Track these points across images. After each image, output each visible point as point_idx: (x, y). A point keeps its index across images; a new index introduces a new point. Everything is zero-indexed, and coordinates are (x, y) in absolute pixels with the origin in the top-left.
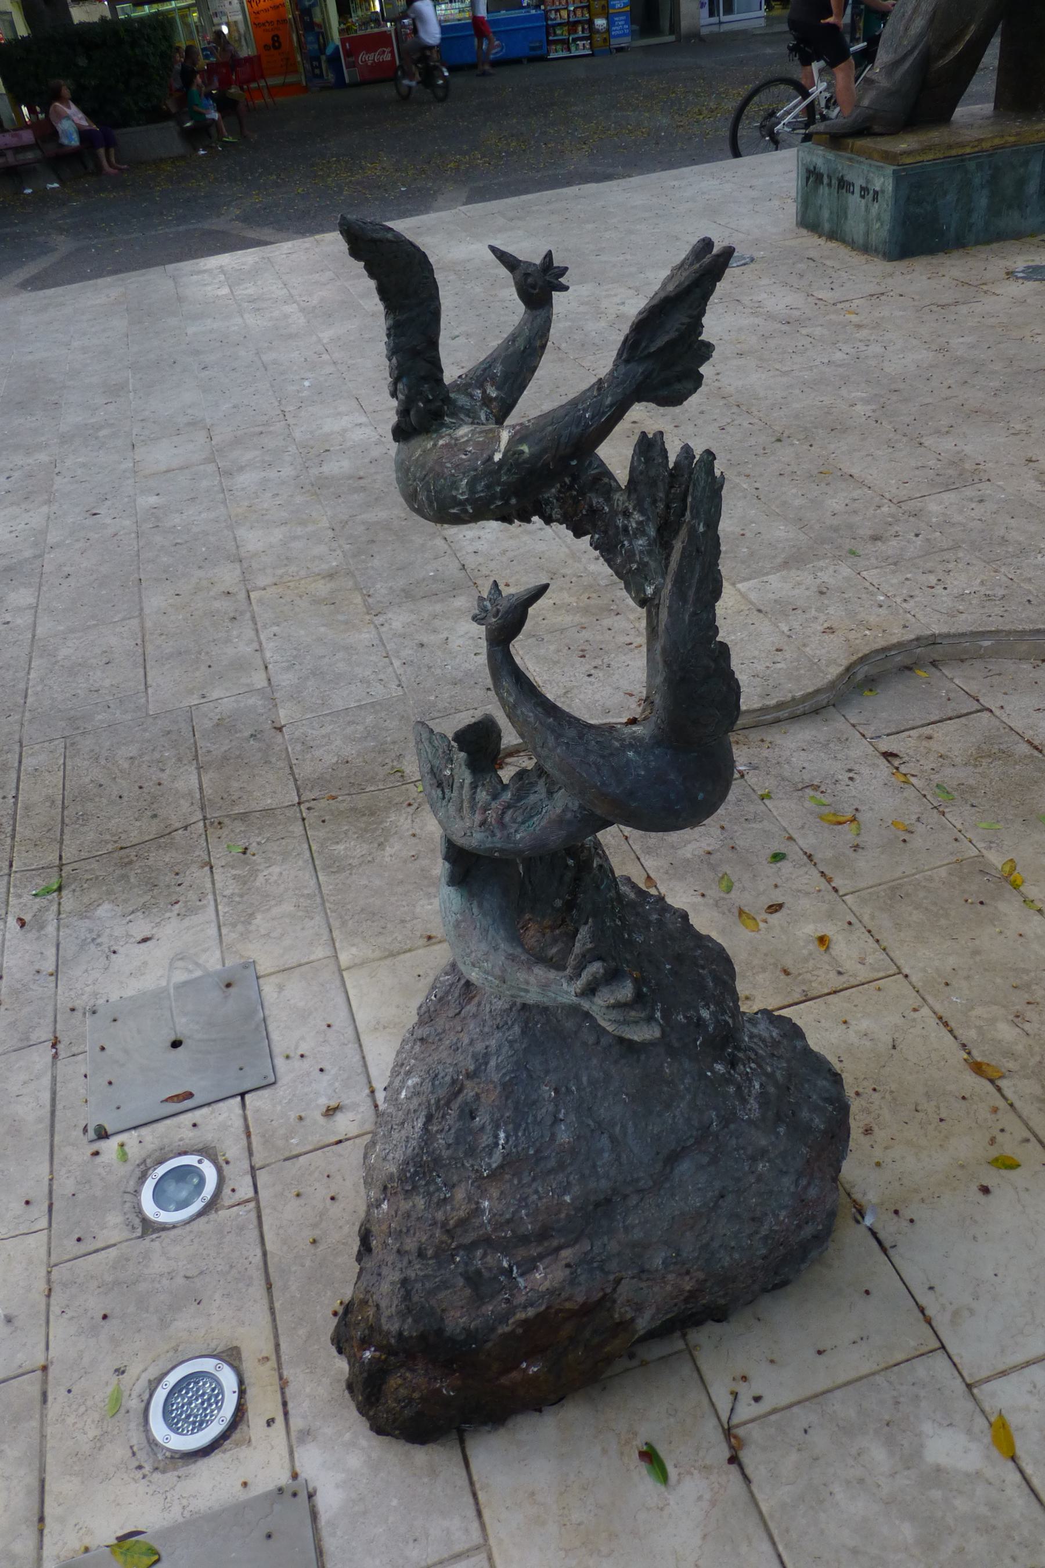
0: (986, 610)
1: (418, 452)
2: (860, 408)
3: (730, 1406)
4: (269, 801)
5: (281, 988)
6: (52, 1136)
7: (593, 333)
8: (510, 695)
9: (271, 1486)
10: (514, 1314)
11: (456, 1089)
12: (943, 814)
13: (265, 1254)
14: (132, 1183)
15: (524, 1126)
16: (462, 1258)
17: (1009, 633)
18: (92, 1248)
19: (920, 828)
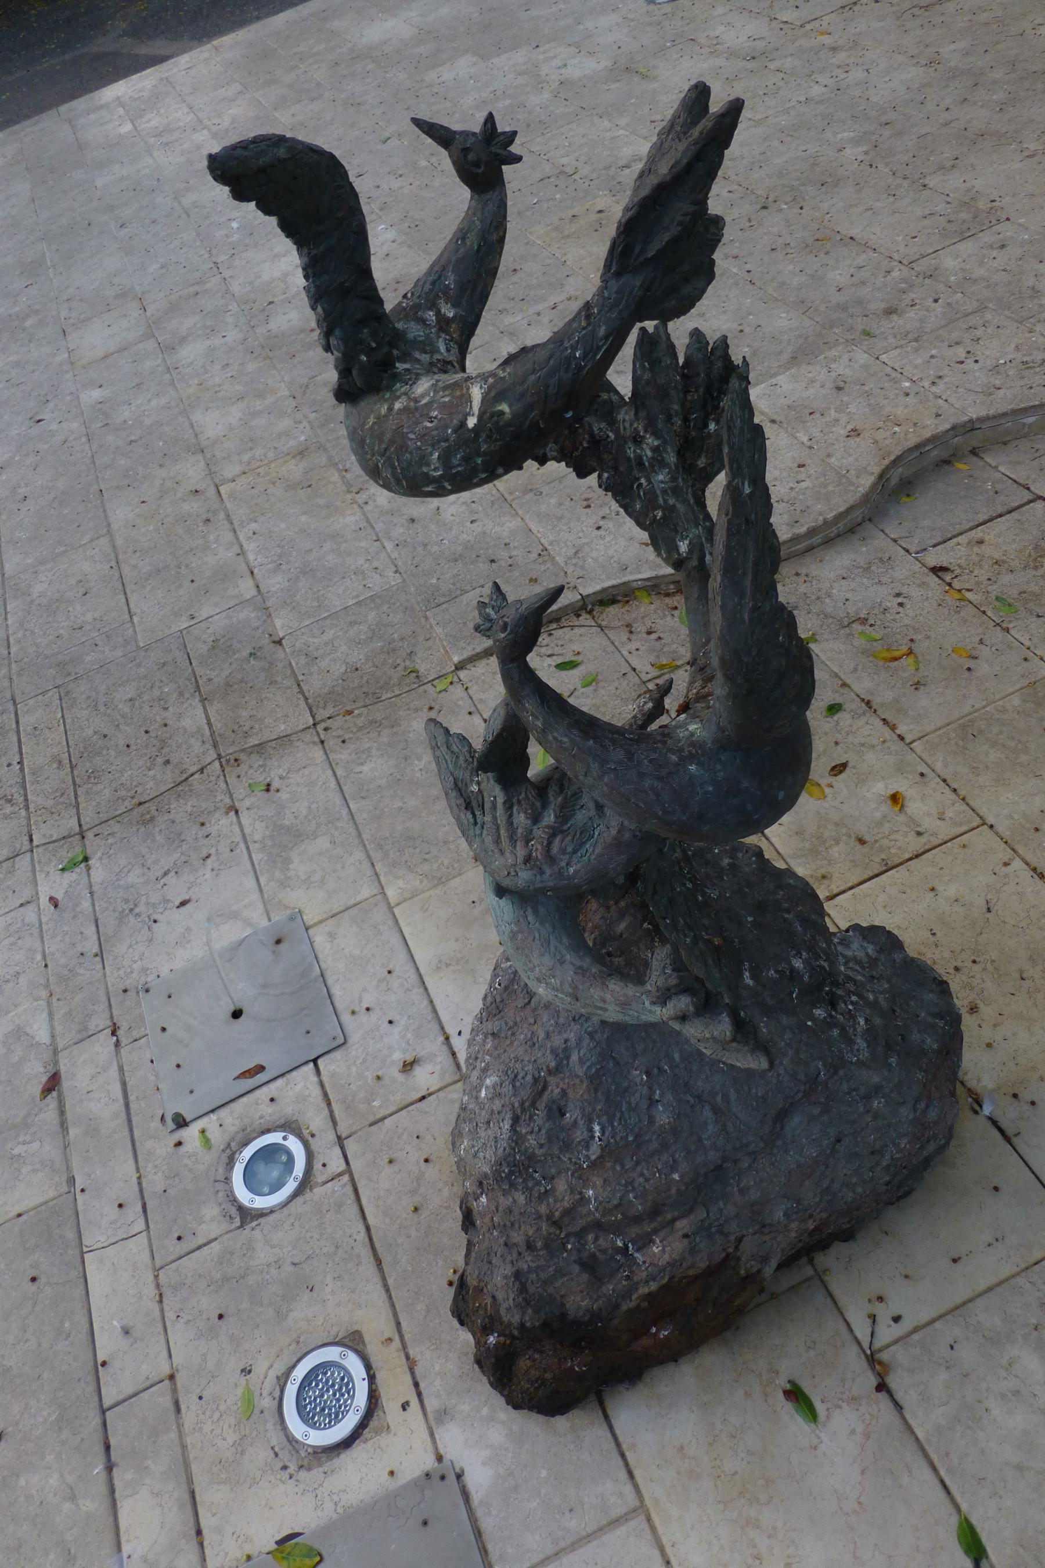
1: (371, 420)
2: (849, 152)
4: (283, 728)
5: (332, 936)
6: (131, 1130)
7: (538, 108)
8: (536, 718)
9: (418, 1472)
10: (637, 1289)
11: (540, 1086)
12: (1007, 630)
13: (368, 1229)
14: (221, 1170)
15: (618, 1115)
18: (194, 1246)
19: (985, 652)
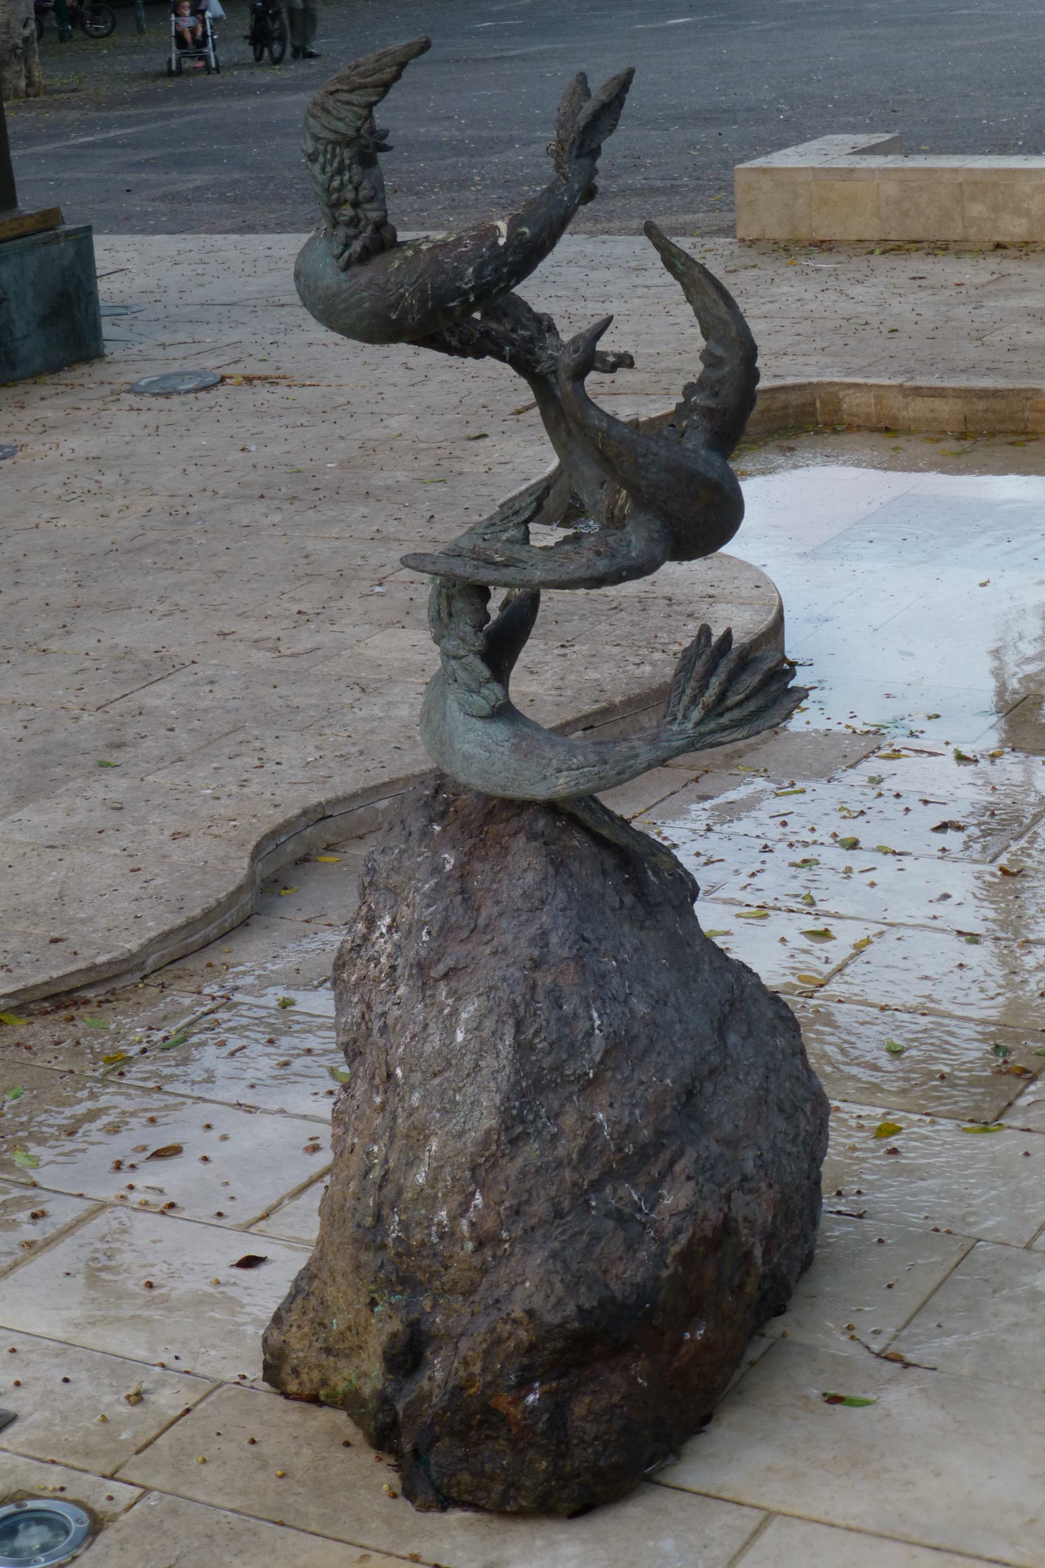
16: (596, 1199)
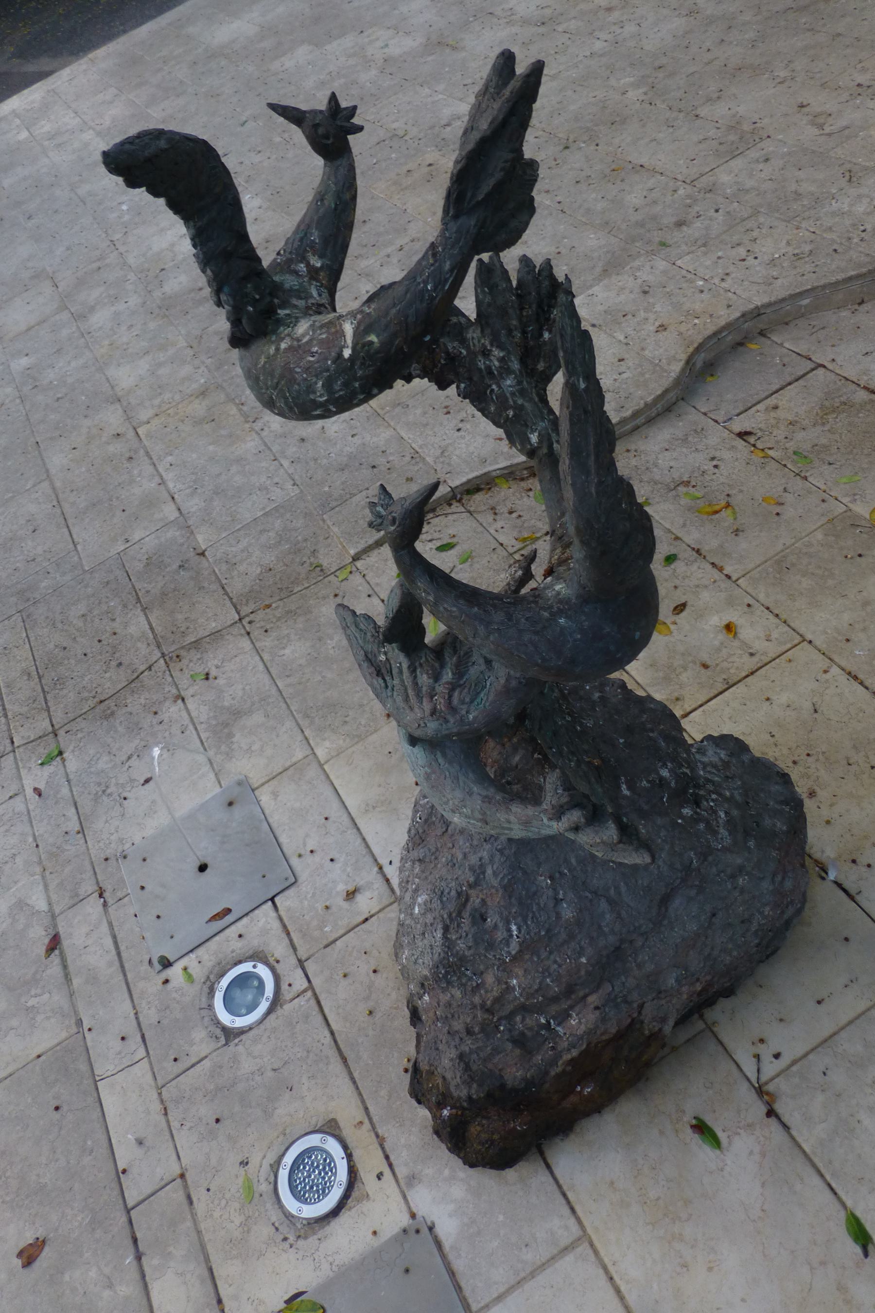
0: (798, 270)
1: (263, 360)
2: (630, 94)
3: (756, 1068)
4: (214, 625)
5: (275, 795)
6: (125, 975)
7: (368, 84)
9: (396, 1229)
11: (463, 899)
12: (806, 478)
13: (332, 1033)
14: (204, 999)
15: (531, 915)
16: (505, 1026)
17: (824, 287)
19: (789, 498)
